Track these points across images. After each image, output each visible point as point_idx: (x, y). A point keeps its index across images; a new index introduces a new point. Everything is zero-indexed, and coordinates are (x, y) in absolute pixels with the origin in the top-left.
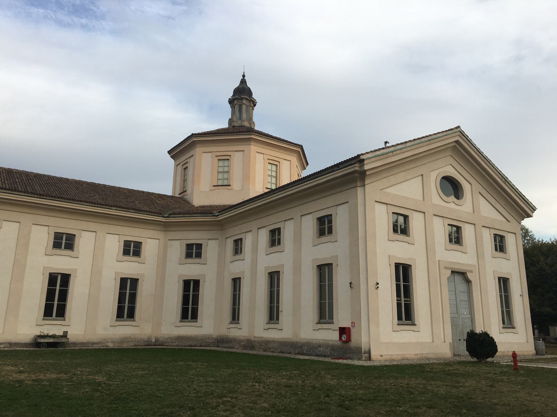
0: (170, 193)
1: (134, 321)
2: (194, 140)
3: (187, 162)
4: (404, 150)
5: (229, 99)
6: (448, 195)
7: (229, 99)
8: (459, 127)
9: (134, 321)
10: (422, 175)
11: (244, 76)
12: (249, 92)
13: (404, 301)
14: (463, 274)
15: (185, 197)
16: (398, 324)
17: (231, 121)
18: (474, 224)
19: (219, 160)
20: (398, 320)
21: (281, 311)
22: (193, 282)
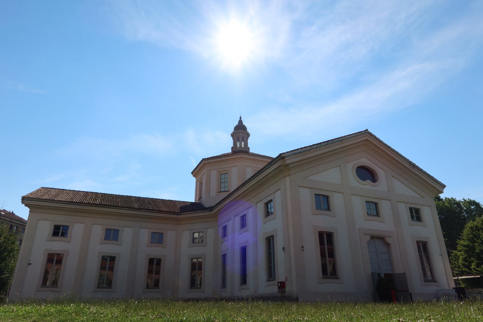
0: (194, 201)
1: (159, 288)
2: (204, 162)
3: (202, 179)
4: (319, 149)
5: (231, 134)
6: (364, 180)
7: (231, 134)
8: (367, 130)
9: (159, 288)
10: (340, 166)
11: (241, 118)
12: (244, 128)
13: (326, 260)
14: (382, 239)
15: (201, 202)
16: (323, 278)
17: (232, 148)
18: (343, 193)
19: (221, 174)
20: (323, 275)
21: (248, 275)
22: (20, 220)
